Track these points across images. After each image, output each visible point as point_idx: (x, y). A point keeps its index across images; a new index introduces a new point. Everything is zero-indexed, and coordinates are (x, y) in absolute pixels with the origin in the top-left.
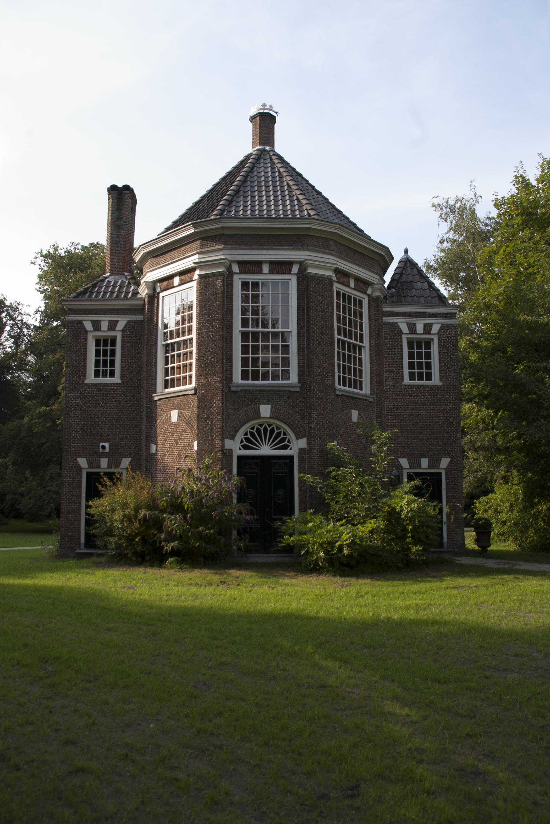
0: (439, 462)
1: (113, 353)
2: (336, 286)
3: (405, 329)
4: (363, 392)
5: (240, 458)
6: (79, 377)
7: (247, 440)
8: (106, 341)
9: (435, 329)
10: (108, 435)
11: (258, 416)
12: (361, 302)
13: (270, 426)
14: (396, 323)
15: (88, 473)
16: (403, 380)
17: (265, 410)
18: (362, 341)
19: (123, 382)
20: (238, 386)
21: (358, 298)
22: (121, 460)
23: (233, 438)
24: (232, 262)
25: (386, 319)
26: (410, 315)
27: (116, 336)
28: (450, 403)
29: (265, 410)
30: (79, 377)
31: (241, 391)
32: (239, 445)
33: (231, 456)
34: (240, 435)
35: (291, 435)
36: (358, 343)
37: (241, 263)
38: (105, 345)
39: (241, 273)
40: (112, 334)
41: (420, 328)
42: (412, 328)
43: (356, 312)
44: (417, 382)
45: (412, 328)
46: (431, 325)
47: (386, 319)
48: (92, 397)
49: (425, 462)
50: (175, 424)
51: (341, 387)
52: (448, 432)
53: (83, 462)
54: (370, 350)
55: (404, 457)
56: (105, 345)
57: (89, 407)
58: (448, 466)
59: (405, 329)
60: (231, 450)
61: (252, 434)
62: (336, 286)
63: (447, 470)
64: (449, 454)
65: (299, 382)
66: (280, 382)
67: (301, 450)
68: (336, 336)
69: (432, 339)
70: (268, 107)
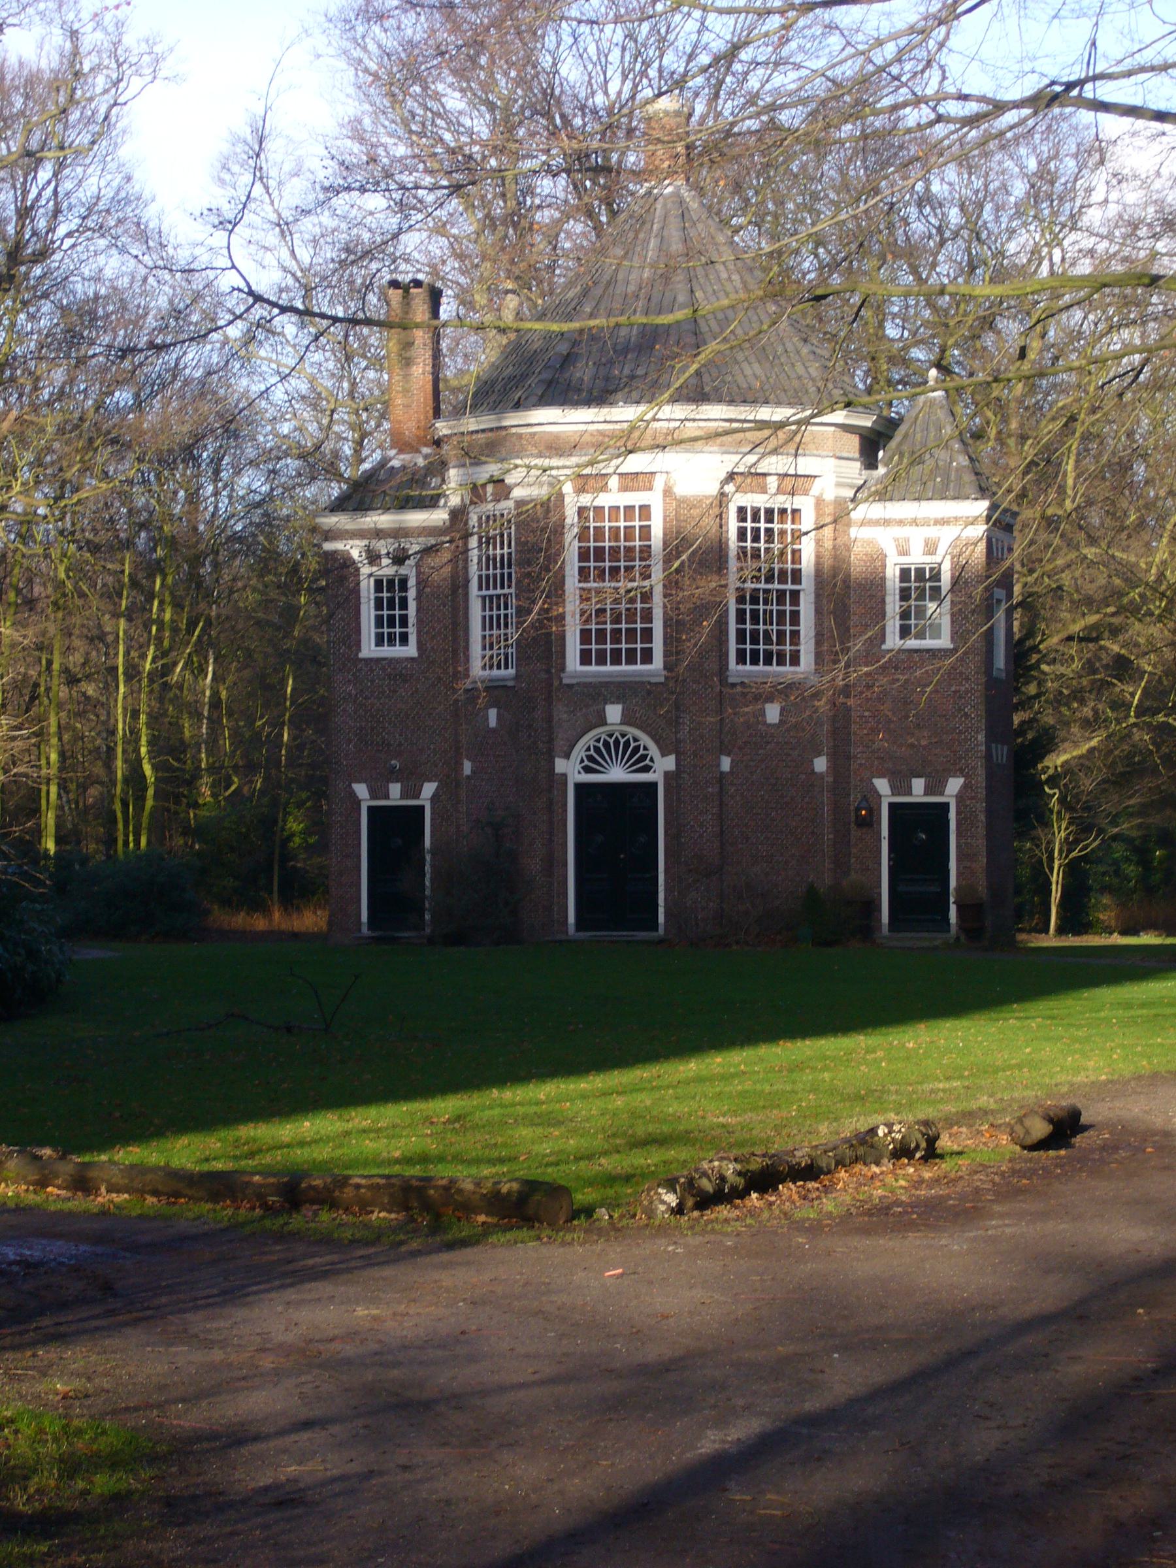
0: (943, 784)
5: (579, 787)
6: (350, 647)
10: (400, 745)
11: (603, 722)
13: (611, 736)
16: (884, 642)
19: (420, 655)
20: (576, 674)
23: (567, 756)
28: (967, 679)
29: (614, 712)
30: (350, 647)
31: (578, 684)
32: (578, 767)
33: (565, 784)
34: (579, 751)
35: (654, 751)
48: (372, 681)
50: (494, 730)
52: (960, 732)
53: (361, 790)
55: (882, 776)
57: (366, 698)
58: (960, 791)
60: (565, 775)
61: (597, 750)
63: (960, 798)
65: (665, 668)
66: (639, 667)
67: (667, 774)
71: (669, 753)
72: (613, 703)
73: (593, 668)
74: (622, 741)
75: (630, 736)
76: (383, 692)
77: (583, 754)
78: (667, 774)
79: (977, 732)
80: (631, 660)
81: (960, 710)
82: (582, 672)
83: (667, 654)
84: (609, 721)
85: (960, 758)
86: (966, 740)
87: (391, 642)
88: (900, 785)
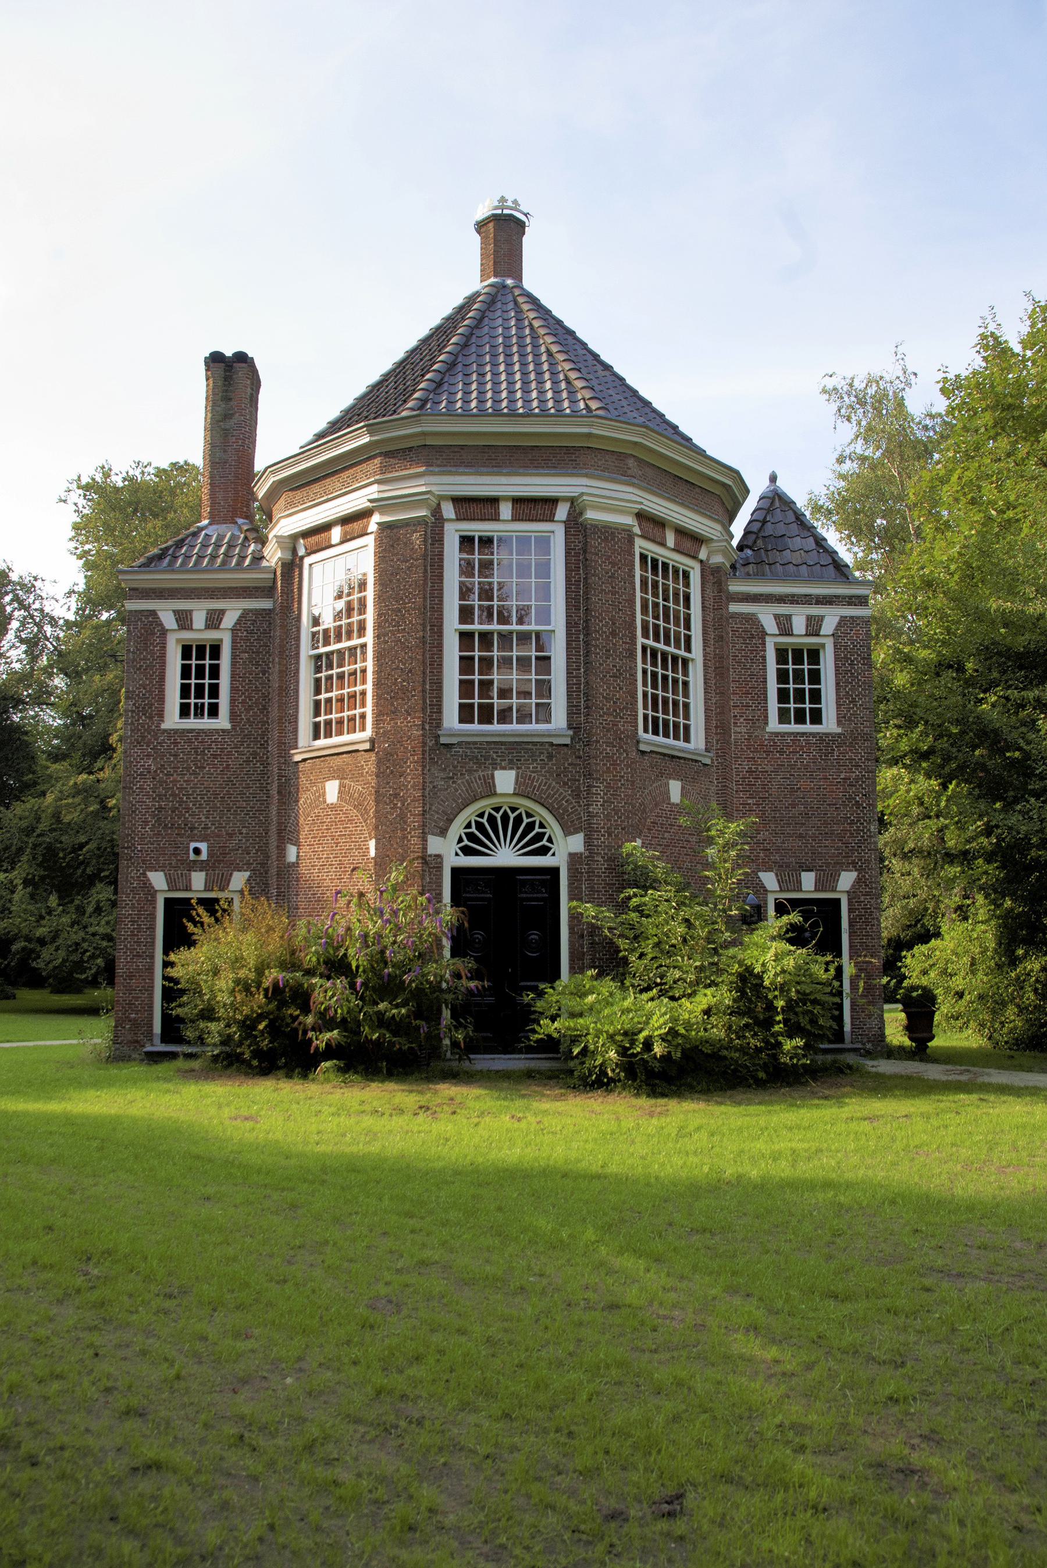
0: (835, 878)
1: (215, 672)
2: (641, 545)
3: (770, 625)
4: (691, 746)
5: (456, 872)
6: (151, 718)
7: (471, 837)
8: (201, 649)
9: (829, 626)
10: (206, 828)
11: (490, 791)
12: (686, 575)
14: (753, 614)
15: (167, 900)
16: (767, 724)
17: (505, 780)
18: (688, 649)
19: (234, 727)
21: (533, 534)
22: (231, 875)
23: (443, 832)
24: (441, 498)
25: (734, 608)
26: (781, 599)
27: (221, 640)
28: (857, 766)
29: (505, 780)
30: (151, 718)
31: (460, 744)
32: (455, 847)
34: (457, 829)
35: (554, 828)
36: (682, 653)
37: (457, 501)
38: (201, 656)
39: (459, 519)
40: (212, 635)
41: (799, 625)
42: (785, 626)
43: (678, 595)
44: (793, 727)
45: (785, 626)
46: (821, 618)
47: (734, 608)
48: (176, 755)
49: (808, 880)
50: (332, 807)
51: (650, 736)
53: (158, 880)
54: (705, 665)
55: (769, 869)
56: (201, 656)
57: (169, 774)
59: (770, 625)
62: (641, 545)
63: (851, 894)
64: (854, 863)
67: (573, 858)
68: (640, 640)
69: (823, 645)
70: (510, 203)
71: (576, 832)
72: (504, 768)
73: (476, 727)
74: (512, 816)
75: (522, 810)
76: (188, 768)
77: (462, 832)
78: (573, 858)
79: (869, 823)
80: (524, 718)
81: (850, 798)
82: (459, 730)
83: (572, 711)
84: (499, 790)
85: (853, 850)
86: (858, 830)
87: (199, 712)
88: (789, 879)
